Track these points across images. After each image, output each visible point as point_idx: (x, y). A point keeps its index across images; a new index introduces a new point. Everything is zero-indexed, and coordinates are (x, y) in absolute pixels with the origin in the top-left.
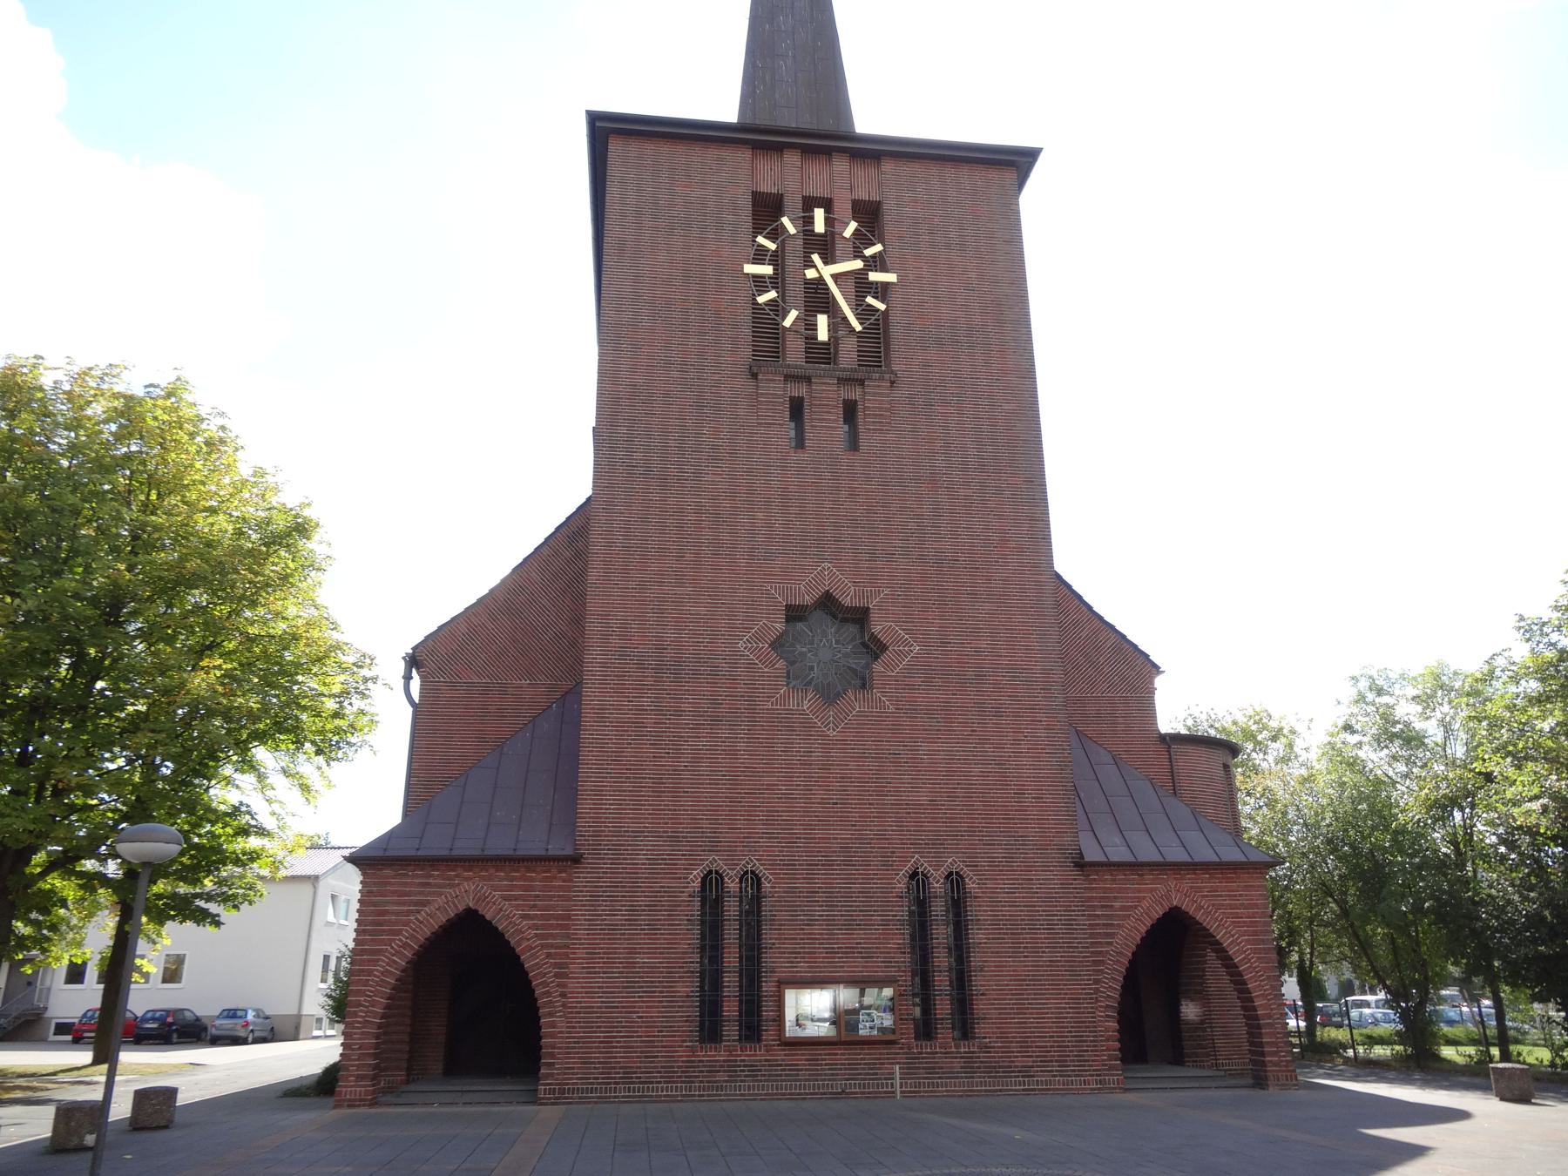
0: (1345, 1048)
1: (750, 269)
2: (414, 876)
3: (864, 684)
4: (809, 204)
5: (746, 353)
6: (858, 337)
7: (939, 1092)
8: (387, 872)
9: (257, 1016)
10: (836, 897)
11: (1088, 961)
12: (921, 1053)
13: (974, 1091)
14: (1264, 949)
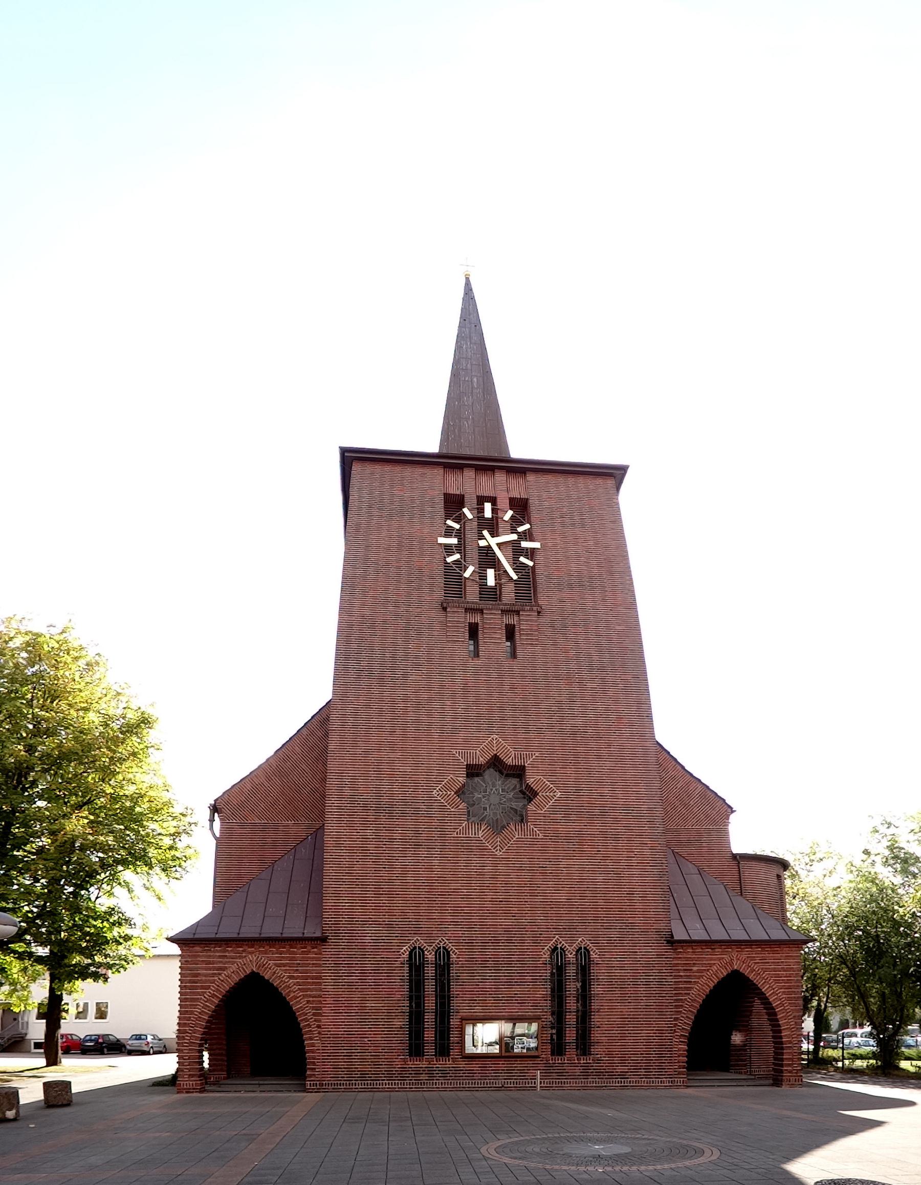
0: (836, 1060)
1: (442, 540)
2: (214, 952)
3: (522, 819)
4: (481, 500)
5: (439, 594)
6: (515, 584)
7: (566, 1087)
8: (197, 948)
9: (154, 1039)
10: (501, 964)
11: (672, 1006)
12: (555, 1063)
13: (588, 1086)
14: (795, 997)
